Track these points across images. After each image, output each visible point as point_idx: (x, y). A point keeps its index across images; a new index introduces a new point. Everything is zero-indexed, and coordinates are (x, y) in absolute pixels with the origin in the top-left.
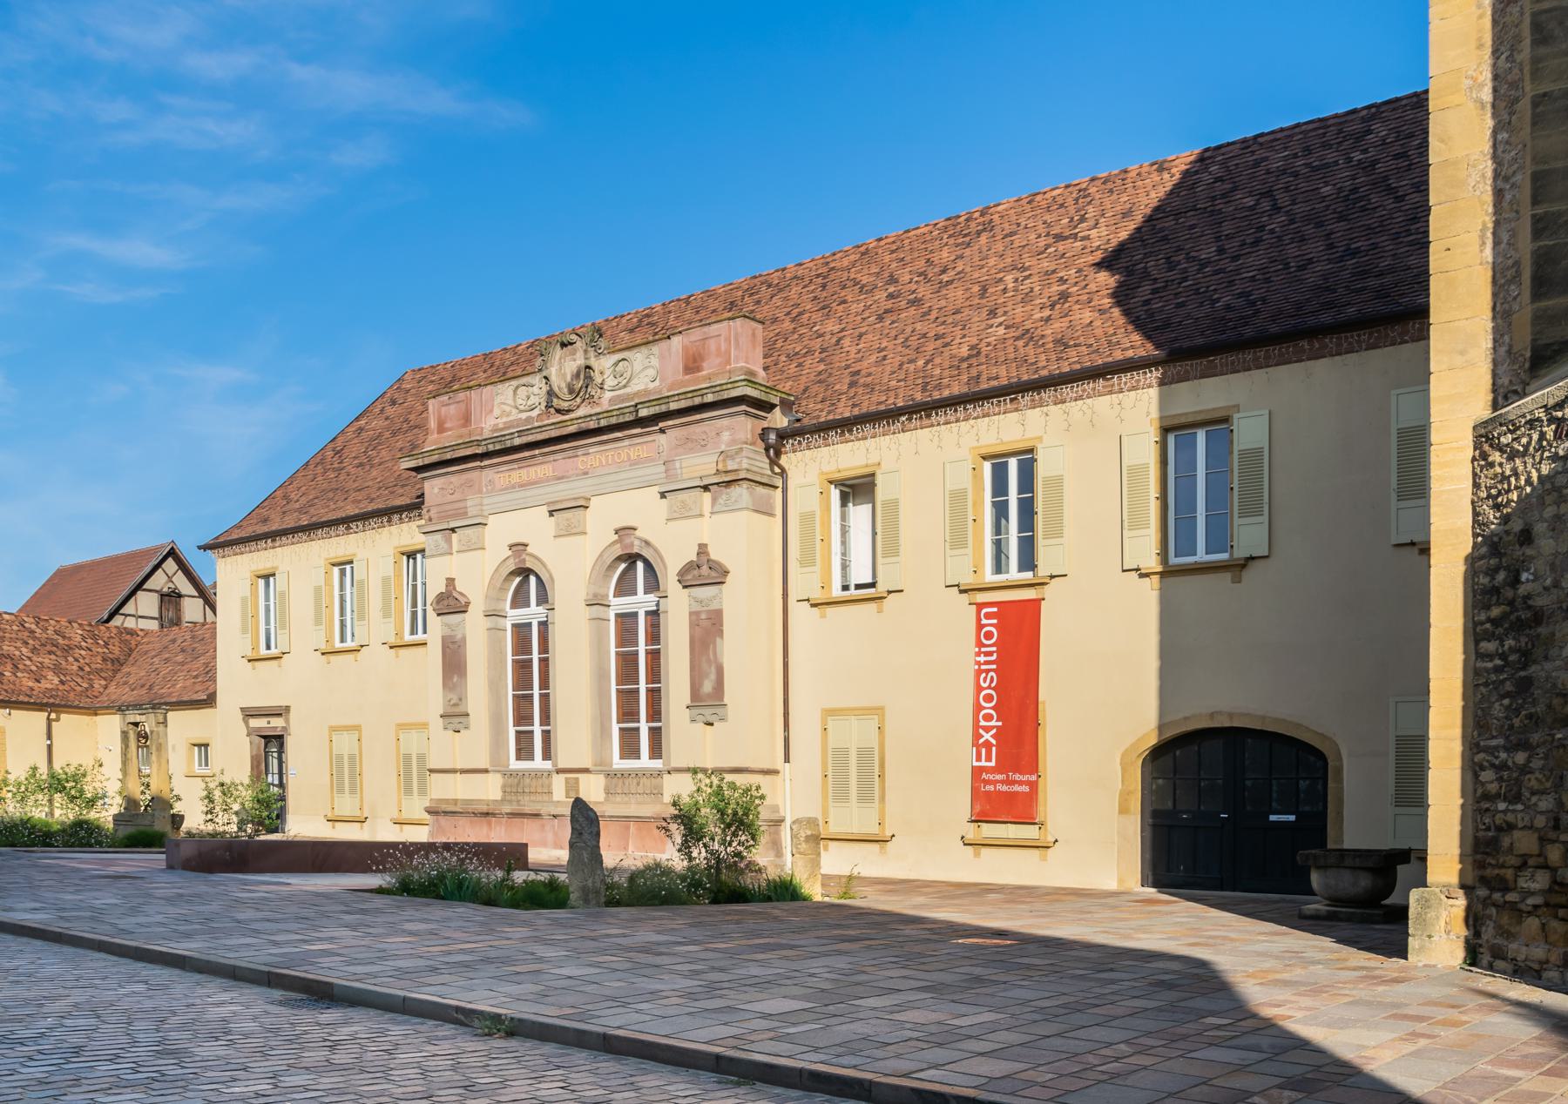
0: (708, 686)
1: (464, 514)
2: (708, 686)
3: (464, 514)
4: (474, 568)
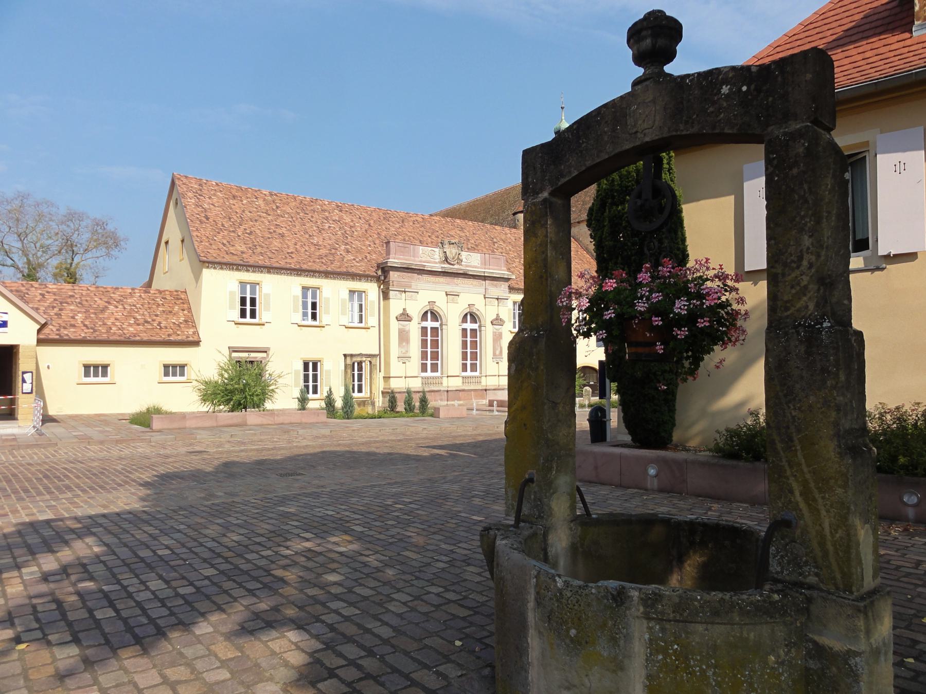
0: (498, 353)
1: (410, 287)
2: (498, 353)
3: (410, 287)
4: (416, 308)
